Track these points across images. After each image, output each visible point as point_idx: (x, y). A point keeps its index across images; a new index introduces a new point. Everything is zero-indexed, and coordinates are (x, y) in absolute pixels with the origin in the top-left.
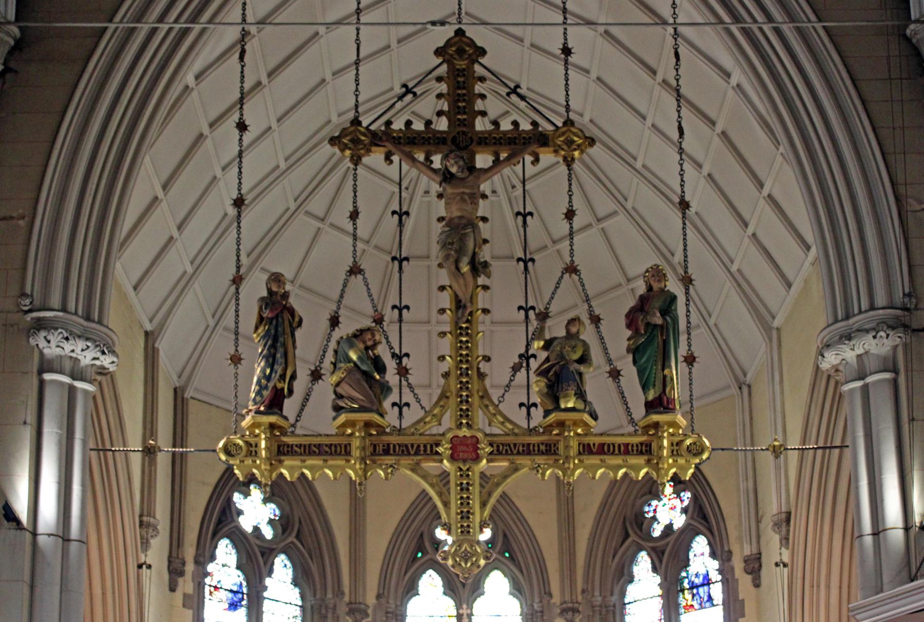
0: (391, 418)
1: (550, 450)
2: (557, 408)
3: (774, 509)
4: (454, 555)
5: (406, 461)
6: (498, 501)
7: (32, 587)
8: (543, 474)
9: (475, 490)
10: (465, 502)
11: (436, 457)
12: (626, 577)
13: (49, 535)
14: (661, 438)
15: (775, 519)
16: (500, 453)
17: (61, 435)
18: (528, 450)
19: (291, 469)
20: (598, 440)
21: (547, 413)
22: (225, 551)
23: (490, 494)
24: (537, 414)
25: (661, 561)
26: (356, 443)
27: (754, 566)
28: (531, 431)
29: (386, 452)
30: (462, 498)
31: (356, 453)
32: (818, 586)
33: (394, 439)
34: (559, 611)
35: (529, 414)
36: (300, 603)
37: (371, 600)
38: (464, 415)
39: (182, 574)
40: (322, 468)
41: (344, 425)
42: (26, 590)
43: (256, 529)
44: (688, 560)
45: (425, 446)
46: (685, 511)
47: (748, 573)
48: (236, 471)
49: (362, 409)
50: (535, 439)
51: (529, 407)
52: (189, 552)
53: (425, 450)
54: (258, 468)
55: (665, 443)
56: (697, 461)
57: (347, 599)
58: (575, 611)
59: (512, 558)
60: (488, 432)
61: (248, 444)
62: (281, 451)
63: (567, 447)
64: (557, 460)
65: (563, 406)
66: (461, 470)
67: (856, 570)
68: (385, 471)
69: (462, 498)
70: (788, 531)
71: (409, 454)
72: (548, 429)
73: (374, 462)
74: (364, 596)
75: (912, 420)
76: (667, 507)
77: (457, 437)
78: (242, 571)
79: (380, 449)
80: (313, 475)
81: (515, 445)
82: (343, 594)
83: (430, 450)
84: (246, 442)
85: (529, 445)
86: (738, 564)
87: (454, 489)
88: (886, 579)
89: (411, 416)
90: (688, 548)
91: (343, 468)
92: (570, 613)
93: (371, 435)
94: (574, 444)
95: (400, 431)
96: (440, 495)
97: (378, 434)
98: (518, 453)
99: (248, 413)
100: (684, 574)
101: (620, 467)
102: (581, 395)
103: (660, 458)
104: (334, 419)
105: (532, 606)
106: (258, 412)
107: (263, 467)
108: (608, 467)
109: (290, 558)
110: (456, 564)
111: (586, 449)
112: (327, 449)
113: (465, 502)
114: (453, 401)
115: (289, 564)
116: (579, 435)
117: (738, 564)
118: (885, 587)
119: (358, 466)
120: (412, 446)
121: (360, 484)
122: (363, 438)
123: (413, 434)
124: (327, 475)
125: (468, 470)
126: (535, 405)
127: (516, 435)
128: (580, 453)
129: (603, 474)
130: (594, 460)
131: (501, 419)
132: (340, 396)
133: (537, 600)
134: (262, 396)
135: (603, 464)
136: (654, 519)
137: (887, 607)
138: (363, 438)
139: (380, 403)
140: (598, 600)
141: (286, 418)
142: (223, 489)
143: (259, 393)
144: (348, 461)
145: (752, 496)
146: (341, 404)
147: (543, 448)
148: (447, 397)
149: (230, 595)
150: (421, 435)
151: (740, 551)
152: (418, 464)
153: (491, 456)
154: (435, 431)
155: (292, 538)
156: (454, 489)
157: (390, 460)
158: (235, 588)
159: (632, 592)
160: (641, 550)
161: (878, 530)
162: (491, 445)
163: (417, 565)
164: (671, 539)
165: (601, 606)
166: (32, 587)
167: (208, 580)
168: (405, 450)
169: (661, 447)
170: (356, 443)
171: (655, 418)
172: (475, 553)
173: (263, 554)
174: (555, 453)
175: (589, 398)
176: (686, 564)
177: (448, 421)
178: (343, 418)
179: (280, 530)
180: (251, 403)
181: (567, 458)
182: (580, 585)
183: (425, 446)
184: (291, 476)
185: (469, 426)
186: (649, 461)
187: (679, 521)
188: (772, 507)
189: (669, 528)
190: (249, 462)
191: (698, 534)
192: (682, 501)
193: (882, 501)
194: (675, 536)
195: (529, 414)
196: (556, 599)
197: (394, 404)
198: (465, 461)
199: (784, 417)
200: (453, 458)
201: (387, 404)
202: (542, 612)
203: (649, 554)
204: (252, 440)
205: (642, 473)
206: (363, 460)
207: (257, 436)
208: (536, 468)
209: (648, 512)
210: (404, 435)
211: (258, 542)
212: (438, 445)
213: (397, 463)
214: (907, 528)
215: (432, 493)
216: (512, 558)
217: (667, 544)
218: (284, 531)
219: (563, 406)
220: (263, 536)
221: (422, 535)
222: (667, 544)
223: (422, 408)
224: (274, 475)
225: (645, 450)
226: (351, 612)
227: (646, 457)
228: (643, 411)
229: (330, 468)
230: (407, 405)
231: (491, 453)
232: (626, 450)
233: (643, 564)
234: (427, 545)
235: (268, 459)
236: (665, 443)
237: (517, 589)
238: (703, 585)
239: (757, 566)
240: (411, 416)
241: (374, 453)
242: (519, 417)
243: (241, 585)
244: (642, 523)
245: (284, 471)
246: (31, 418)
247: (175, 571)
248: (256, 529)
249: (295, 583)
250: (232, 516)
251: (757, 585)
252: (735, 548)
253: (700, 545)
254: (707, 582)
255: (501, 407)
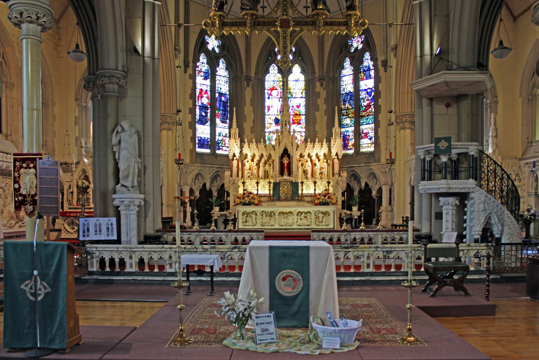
0: (260, 12)
1: (313, 24)
2: (316, 9)
3: (392, 44)
4: (281, 62)
5: (265, 28)
6: (298, 39)
7: (144, 75)
8: (311, 33)
9: (288, 38)
10: (285, 43)
11: (275, 26)
12: (341, 67)
13: (148, 57)
14: (351, 20)
15: (392, 47)
16: (297, 25)
17: (151, 21)
18: (306, 24)
19: (226, 31)
20: (330, 20)
21: (313, 10)
22: (203, 59)
23: (293, 40)
24: (310, 10)
25: (353, 61)
26: (248, 21)
27: (385, 64)
28: (308, 17)
29: (258, 25)
30: (284, 41)
31: (248, 25)
32: (405, 73)
33: (261, 20)
34: (318, 79)
35: (307, 10)
36: (228, 76)
37: (253, 75)
38: (285, 11)
39: (188, 67)
40: (237, 31)
41: (244, 15)
42: (142, 77)
43: (213, 49)
44: (363, 61)
45: (272, 22)
46: (362, 42)
47: (383, 67)
48: (208, 32)
49: (250, 9)
50: (309, 20)
51: (307, 8)
52: (191, 59)
53: (272, 24)
54: (215, 31)
55: (353, 22)
56: (363, 28)
57: (244, 75)
58: (323, 79)
59: (302, 59)
60: (294, 17)
61: (212, 22)
62: (223, 25)
63: (320, 23)
64: (316, 28)
65: (318, 8)
66: (284, 31)
67: (414, 70)
68: (258, 31)
69: (284, 41)
70: (396, 52)
71: (266, 25)
72: (314, 15)
73: (254, 28)
74: (251, 73)
75: (435, 16)
76: (356, 41)
77: (282, 19)
78: (209, 65)
79: (256, 23)
80: (234, 33)
81: (302, 22)
82: (243, 73)
83: (273, 24)
84: (212, 22)
85: (307, 22)
86: (379, 63)
87: (281, 38)
88: (424, 73)
89: (267, 11)
90: (363, 57)
91: (244, 31)
92: (322, 80)
93: (253, 18)
94: (322, 21)
95: (263, 17)
96: (277, 40)
97: (256, 18)
98: (303, 25)
99: (212, 11)
100: (361, 66)
101: (337, 30)
102: (325, 4)
103: (351, 27)
104: (241, 12)
105: (309, 77)
106: (215, 11)
107: (217, 30)
108: (333, 30)
109: (225, 60)
110: (282, 65)
111: (326, 24)
112: (239, 24)
113: (285, 43)
114: (281, 6)
115: (225, 62)
116: (323, 18)
117: (379, 63)
118: (423, 76)
119: (249, 30)
120: (267, 22)
121: (250, 36)
122: (251, 19)
123: (268, 18)
124: (239, 33)
125: (286, 31)
126: (309, 7)
127: (302, 18)
128: (324, 25)
129: (331, 33)
130: (328, 28)
131: (297, 12)
132: (243, 4)
133: (310, 75)
134: (217, 4)
135: (331, 29)
136: (352, 45)
137: (421, 84)
138: (251, 19)
139: (257, 7)
140: (331, 75)
141: (225, 12)
142: (202, 35)
143: (216, 3)
144: (246, 28)
145: (385, 38)
146: (243, 7)
147: (311, 23)
148: (279, 4)
149: (205, 74)
150: (270, 18)
151: (381, 58)
152: (269, 29)
153: (294, 26)
154: (275, 17)
155: (225, 52)
156: (281, 38)
157: (260, 27)
158: (206, 71)
159: (344, 72)
160: (347, 57)
161: (422, 55)
162: (294, 22)
163: (269, 61)
164: (357, 53)
165: (332, 78)
166: (144, 75)
167: (197, 69)
168: (265, 24)
169: (351, 23)
170: (248, 21)
171: (350, 12)
172: (288, 61)
173: (216, 58)
174: (315, 25)
175: (328, 5)
176: (362, 62)
177: (279, 13)
178: (244, 12)
179: (221, 49)
180: (213, 7)
181: (319, 27)
182: (325, 70)
183: (272, 22)
184: (227, 34)
185: (286, 15)
186: (347, 28)
187: (360, 47)
188: (392, 42)
189: (356, 48)
190: (213, 29)
191: (366, 51)
192: (361, 39)
193: (424, 45)
194: (359, 52)
195: (307, 10)
196: (317, 75)
197: (261, 7)
198: (285, 28)
199: (397, 9)
200: (281, 27)
201: (259, 7)
202: (312, 79)
203: (349, 58)
204: (214, 21)
205: (345, 33)
206: (251, 27)
207: (215, 19)
208: (309, 31)
209: (350, 43)
210: (265, 18)
211: (214, 54)
212: (276, 22)
213: (262, 28)
214: (431, 55)
215: (274, 39)
216: (302, 59)
217: (356, 55)
218: (223, 50)
219: (318, 8)
220: (216, 52)
221: (270, 51)
222: (356, 55)
223: (271, 8)
224: (221, 33)
225: (346, 24)
226: (246, 80)
227: (346, 27)
228: (345, 10)
229: (239, 30)
230: (266, 7)
231: (294, 25)
232: (339, 24)
233: (347, 63)
234: (272, 54)
235: (219, 27)
236: (353, 22)
237: (303, 71)
238: (367, 71)
239: (386, 64)
240: (267, 11)
241: (254, 25)
242: (304, 12)
243: (208, 70)
244: (347, 47)
245: (225, 32)
246: (141, 15)
247: (186, 65)
248: (213, 49)
249: (227, 69)
250: (205, 44)
251: (386, 71)
252: (379, 57)
253: (367, 56)
254: (369, 69)
255: (298, 8)
